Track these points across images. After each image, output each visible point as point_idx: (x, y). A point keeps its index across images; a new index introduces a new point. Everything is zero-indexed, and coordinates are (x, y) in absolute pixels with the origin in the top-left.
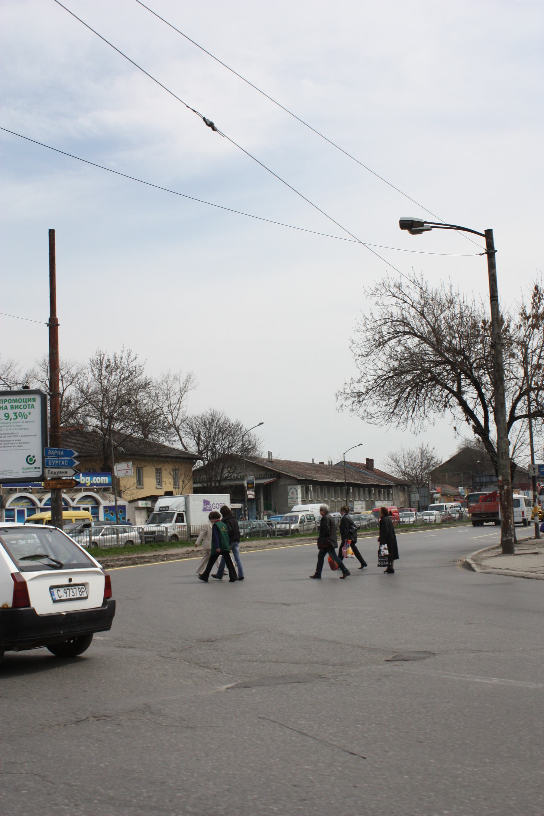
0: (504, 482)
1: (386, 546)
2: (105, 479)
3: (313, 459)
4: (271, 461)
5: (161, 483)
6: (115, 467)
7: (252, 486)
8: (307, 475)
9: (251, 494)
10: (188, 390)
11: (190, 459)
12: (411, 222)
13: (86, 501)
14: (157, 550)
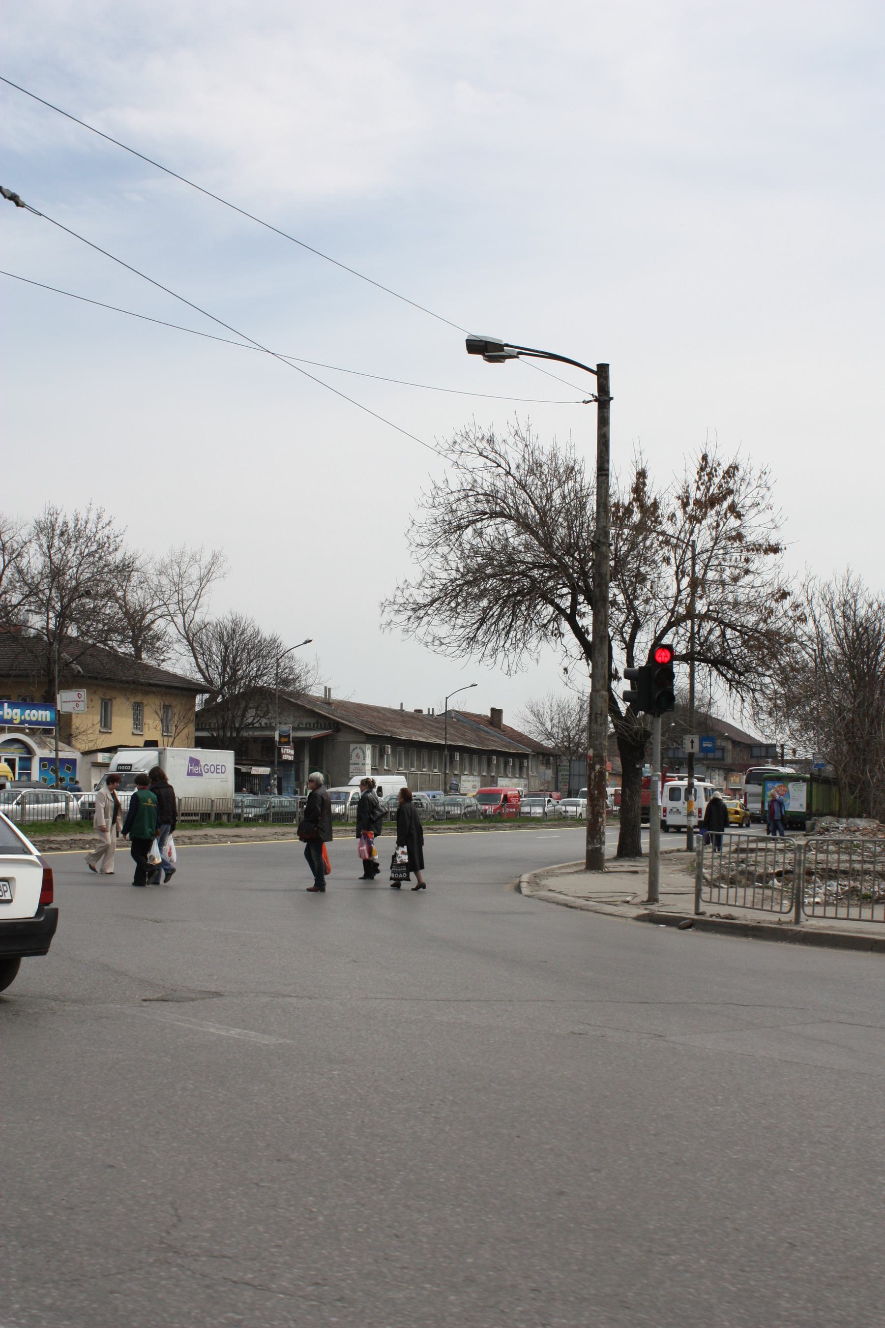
0: (596, 759)
1: (405, 849)
2: (45, 715)
3: (402, 704)
4: (327, 702)
5: (142, 728)
6: (58, 696)
7: (286, 740)
8: (385, 728)
9: (288, 753)
10: (212, 578)
11: (187, 689)
12: (483, 344)
13: (12, 748)
14: (86, 831)
